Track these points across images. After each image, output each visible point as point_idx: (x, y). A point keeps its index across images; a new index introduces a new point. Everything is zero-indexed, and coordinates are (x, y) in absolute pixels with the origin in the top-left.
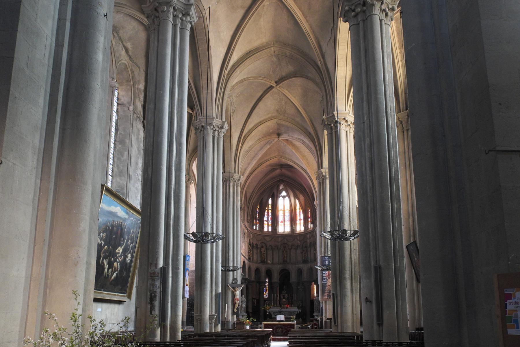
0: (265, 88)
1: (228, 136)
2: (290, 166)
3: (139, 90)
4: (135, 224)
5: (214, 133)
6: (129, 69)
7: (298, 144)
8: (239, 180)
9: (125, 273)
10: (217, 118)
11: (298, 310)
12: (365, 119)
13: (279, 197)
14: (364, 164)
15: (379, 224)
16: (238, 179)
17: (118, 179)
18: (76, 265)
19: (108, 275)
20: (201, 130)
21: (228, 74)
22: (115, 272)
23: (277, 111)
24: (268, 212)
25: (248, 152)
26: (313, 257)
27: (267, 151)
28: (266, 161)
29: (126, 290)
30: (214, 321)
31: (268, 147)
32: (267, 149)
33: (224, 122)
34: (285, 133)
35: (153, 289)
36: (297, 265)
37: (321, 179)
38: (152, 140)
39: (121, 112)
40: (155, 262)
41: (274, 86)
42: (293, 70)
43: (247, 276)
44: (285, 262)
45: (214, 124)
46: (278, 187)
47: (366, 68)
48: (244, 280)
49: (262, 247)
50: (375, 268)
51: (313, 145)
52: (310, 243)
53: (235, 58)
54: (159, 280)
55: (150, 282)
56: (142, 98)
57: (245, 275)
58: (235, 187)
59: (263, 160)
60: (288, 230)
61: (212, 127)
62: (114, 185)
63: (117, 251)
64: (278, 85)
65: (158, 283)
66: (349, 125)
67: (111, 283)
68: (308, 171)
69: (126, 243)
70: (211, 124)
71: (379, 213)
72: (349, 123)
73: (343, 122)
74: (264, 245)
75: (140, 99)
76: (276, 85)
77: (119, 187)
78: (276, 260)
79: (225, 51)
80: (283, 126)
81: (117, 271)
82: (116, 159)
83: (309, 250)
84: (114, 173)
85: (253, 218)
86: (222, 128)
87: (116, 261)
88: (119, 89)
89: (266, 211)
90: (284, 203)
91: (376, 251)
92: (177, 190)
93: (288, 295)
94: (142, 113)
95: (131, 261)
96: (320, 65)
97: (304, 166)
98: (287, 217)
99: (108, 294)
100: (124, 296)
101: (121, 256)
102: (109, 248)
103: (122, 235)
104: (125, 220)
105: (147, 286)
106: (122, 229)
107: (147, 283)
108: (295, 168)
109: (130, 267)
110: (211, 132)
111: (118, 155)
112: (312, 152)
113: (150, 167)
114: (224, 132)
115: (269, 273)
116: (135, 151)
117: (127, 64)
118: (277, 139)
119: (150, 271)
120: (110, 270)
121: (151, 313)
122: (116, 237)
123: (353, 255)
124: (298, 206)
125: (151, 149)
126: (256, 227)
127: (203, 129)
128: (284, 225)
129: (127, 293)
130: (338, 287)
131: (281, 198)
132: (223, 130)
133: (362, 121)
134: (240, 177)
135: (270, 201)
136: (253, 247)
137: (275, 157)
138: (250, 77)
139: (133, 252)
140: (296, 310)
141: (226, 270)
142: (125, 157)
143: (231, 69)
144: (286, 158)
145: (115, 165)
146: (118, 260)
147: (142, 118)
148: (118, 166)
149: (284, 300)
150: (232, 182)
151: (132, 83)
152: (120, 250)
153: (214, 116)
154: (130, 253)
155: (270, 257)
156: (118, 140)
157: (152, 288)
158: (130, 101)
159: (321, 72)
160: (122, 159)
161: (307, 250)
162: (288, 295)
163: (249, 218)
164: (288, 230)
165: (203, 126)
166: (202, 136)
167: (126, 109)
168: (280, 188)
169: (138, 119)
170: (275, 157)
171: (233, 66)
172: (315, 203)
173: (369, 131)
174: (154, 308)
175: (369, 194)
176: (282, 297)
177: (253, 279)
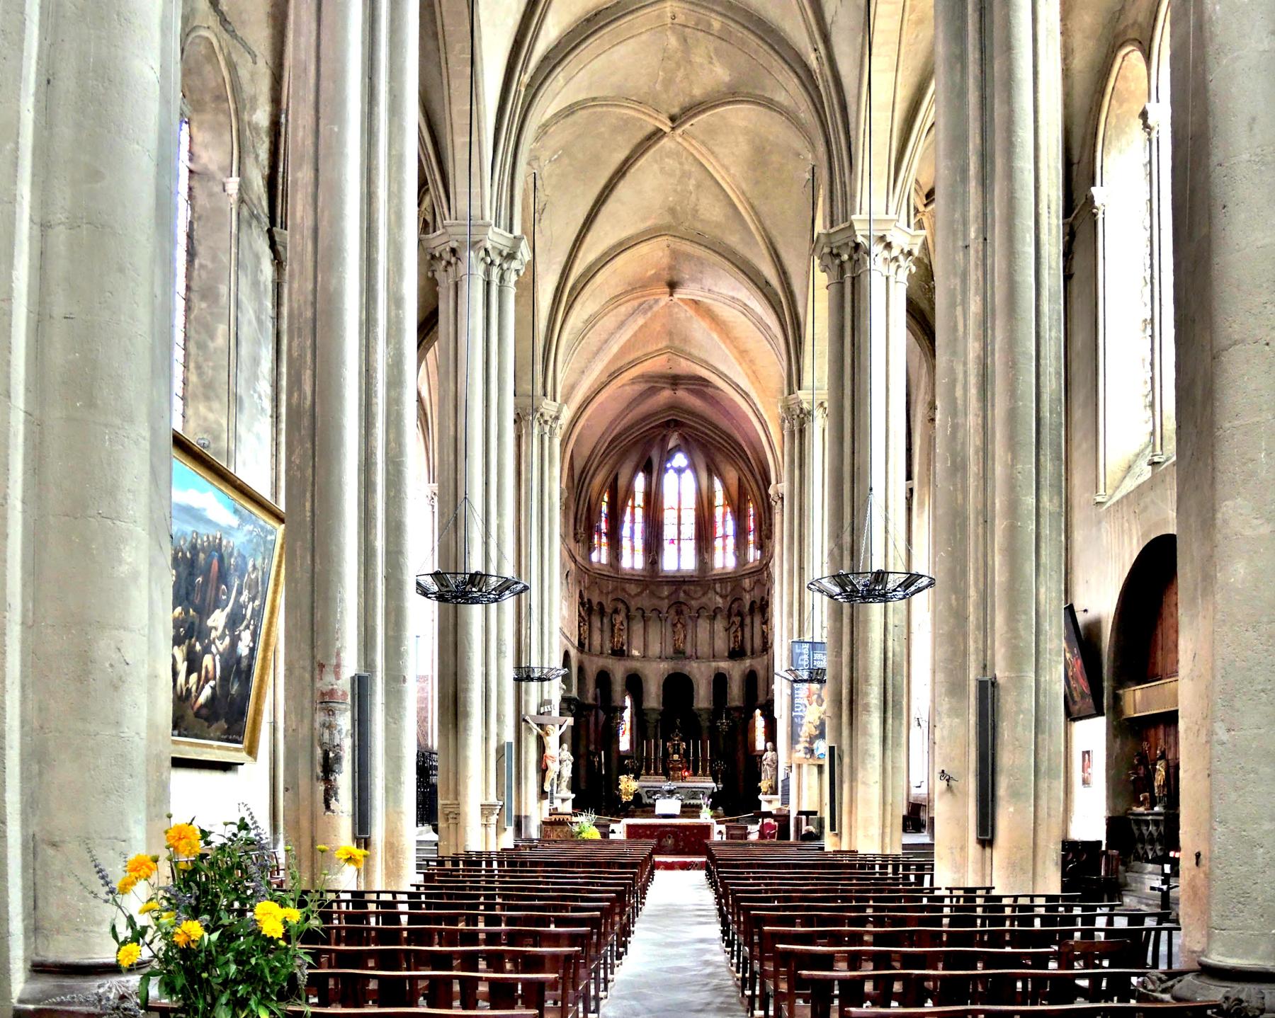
0: (640, 136)
1: (528, 286)
2: (705, 380)
3: (255, 128)
4: (258, 545)
5: (487, 273)
6: (221, 58)
7: (727, 313)
8: (557, 418)
9: (236, 687)
10: (497, 224)
11: (714, 785)
12: (973, 235)
13: (666, 470)
14: (960, 376)
15: (998, 560)
16: (554, 414)
17: (202, 409)
18: (116, 688)
19: (189, 690)
20: (449, 263)
21: (529, 86)
22: (207, 681)
23: (672, 211)
24: (633, 514)
25: (582, 335)
26: (758, 642)
27: (635, 335)
28: (633, 364)
29: (241, 733)
30: (493, 819)
31: (641, 321)
32: (636, 327)
33: (517, 240)
34: (694, 279)
35: (332, 739)
36: (714, 664)
37: (798, 423)
38: (310, 286)
39: (201, 199)
40: (334, 661)
41: (667, 129)
42: (727, 79)
43: (574, 693)
44: (679, 654)
45: (489, 246)
46: (664, 440)
47: (983, 72)
48: (568, 704)
49: (616, 611)
50: (982, 686)
51: (774, 317)
52: (753, 603)
53: (551, 31)
54: (349, 714)
55: (320, 717)
56: (264, 154)
57: (569, 689)
58: (546, 438)
59: (626, 360)
60: (689, 563)
61: (482, 254)
62: (192, 424)
63: (210, 623)
64: (679, 126)
65: (344, 721)
66: (896, 259)
67: (197, 715)
68: (753, 394)
69: (237, 600)
70: (473, 245)
71: (1000, 525)
72: (896, 252)
73: (877, 249)
74: (621, 606)
75: (257, 156)
76: (673, 129)
77: (207, 430)
78: (655, 649)
79: (522, 8)
80: (689, 257)
81: (215, 678)
82: (193, 348)
83: (748, 620)
84: (190, 388)
85: (591, 529)
86: (511, 256)
87: (210, 652)
88: (194, 125)
89: (628, 510)
90: (680, 486)
91: (985, 637)
92: (393, 445)
93: (688, 745)
94: (265, 203)
95: (252, 650)
96: (814, 64)
97: (744, 384)
98: (689, 529)
99: (191, 744)
100: (237, 750)
101: (222, 637)
102: (187, 613)
103: (223, 577)
104: (228, 531)
105: (312, 729)
106: (221, 559)
107: (313, 720)
108: (718, 388)
109: (250, 667)
110: (480, 270)
111: (197, 332)
112: (771, 339)
113: (308, 373)
114: (517, 271)
115: (635, 684)
116: (250, 323)
117: (215, 41)
118: (666, 298)
119: (318, 684)
120: (194, 677)
121: (328, 807)
122: (206, 582)
123: (890, 643)
124: (719, 498)
125: (309, 314)
126: (600, 556)
127: (453, 260)
128: (679, 549)
129: (246, 742)
130: (845, 732)
131: (671, 471)
132: (515, 265)
133: (960, 243)
134: (559, 411)
135: (640, 482)
136: (590, 611)
137: (659, 352)
138: (594, 99)
139: (256, 627)
140: (709, 784)
141: (523, 676)
142: (220, 341)
143: (538, 69)
144: (690, 357)
145: (192, 365)
146: (213, 649)
147: (267, 220)
148: (198, 367)
149: (676, 757)
150: (536, 424)
151: (232, 106)
152: (218, 619)
153: (487, 218)
154: (247, 627)
155: (637, 641)
156: (194, 285)
157: (326, 736)
158: (228, 161)
159: (817, 87)
160: (211, 345)
161: (742, 625)
162: (688, 745)
163: (581, 530)
164: (689, 563)
165: (453, 251)
166: (451, 282)
167: (218, 189)
168: (671, 445)
169: (254, 223)
170: (659, 352)
171: (545, 58)
172: (771, 491)
173: (980, 273)
174: (336, 794)
175: (973, 468)
176: (671, 750)
177: (590, 700)
